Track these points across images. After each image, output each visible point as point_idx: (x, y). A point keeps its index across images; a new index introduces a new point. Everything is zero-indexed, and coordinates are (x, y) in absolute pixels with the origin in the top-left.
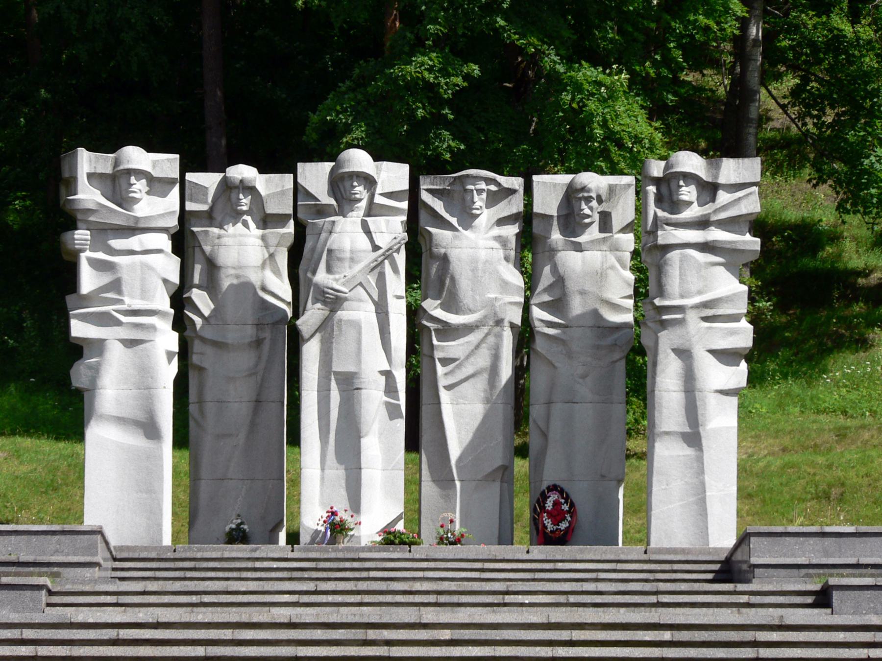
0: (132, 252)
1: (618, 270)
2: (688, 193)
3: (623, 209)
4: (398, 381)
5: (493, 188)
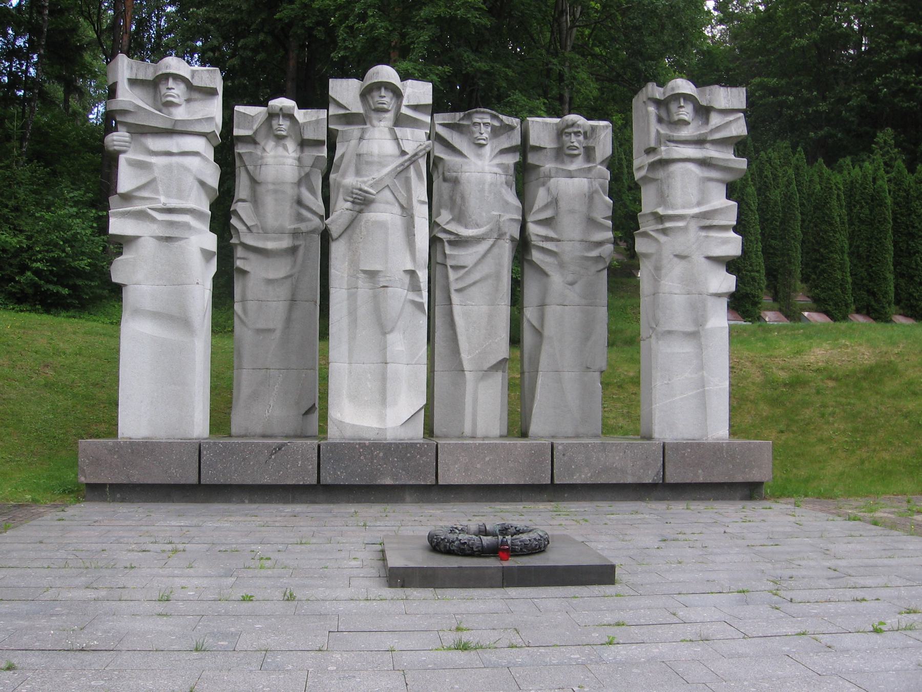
0: (169, 154)
1: (601, 194)
2: (686, 112)
3: (604, 145)
4: (421, 280)
5: (496, 124)
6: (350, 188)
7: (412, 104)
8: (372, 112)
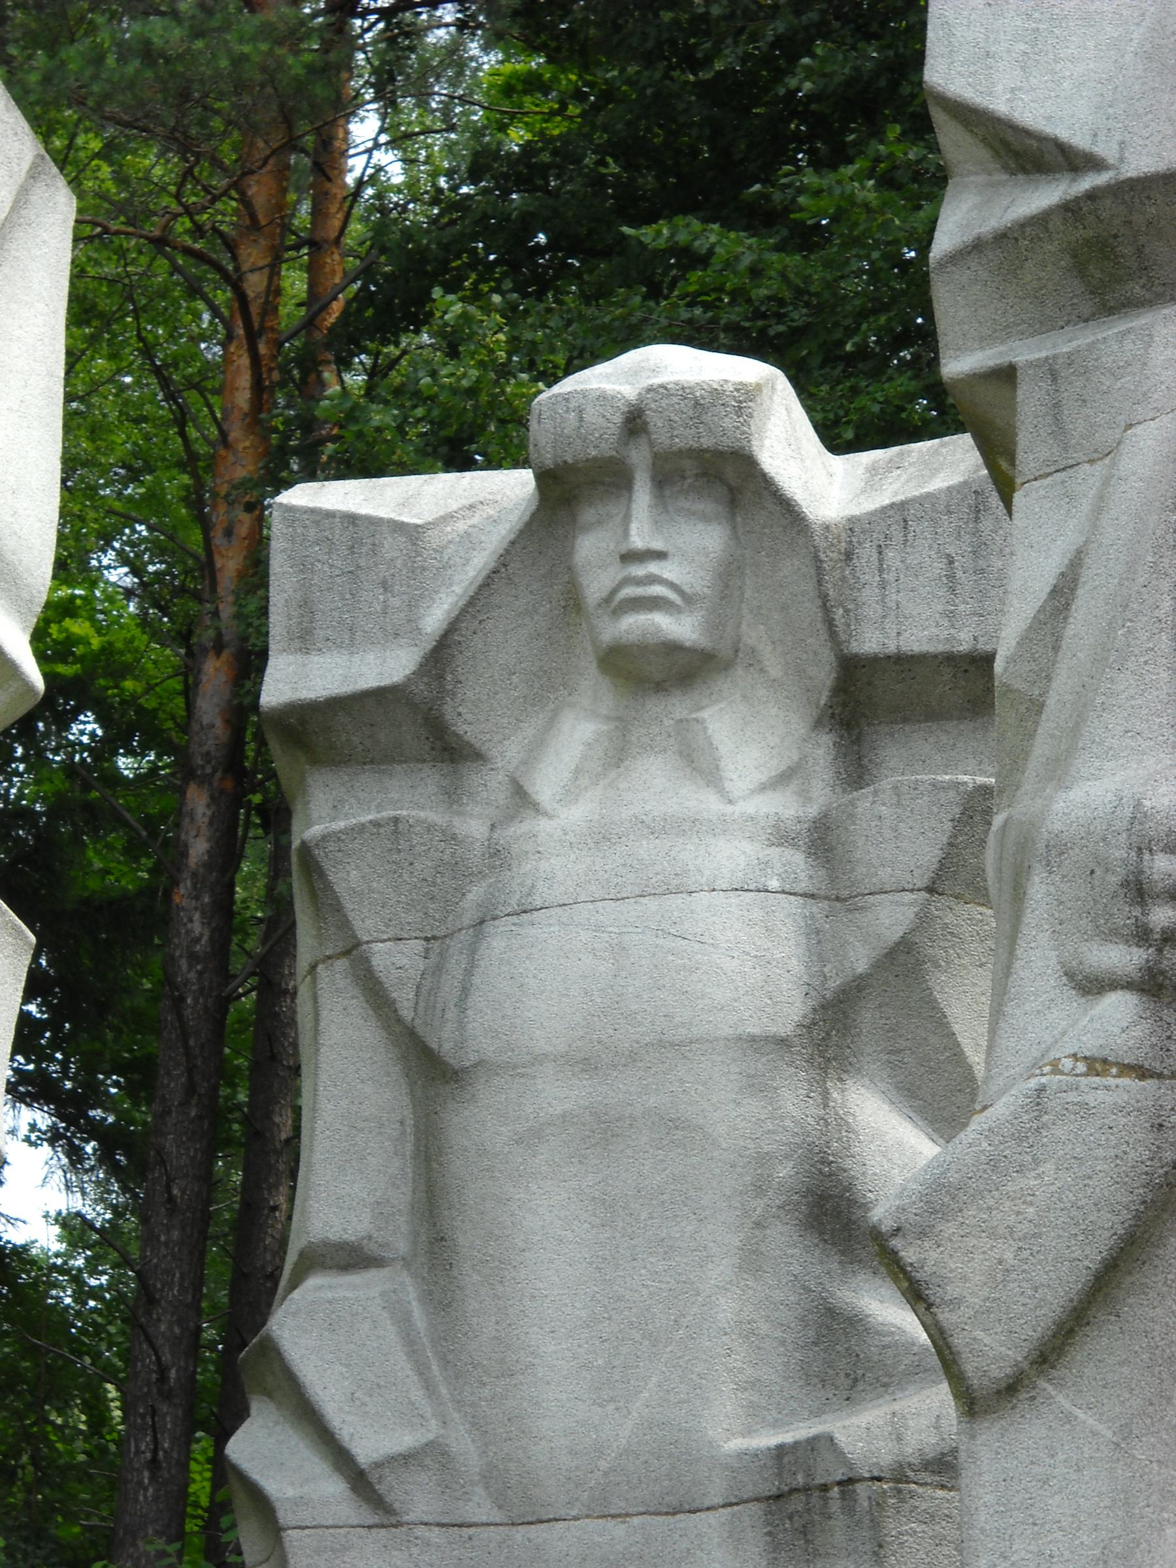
6: (1119, 853)
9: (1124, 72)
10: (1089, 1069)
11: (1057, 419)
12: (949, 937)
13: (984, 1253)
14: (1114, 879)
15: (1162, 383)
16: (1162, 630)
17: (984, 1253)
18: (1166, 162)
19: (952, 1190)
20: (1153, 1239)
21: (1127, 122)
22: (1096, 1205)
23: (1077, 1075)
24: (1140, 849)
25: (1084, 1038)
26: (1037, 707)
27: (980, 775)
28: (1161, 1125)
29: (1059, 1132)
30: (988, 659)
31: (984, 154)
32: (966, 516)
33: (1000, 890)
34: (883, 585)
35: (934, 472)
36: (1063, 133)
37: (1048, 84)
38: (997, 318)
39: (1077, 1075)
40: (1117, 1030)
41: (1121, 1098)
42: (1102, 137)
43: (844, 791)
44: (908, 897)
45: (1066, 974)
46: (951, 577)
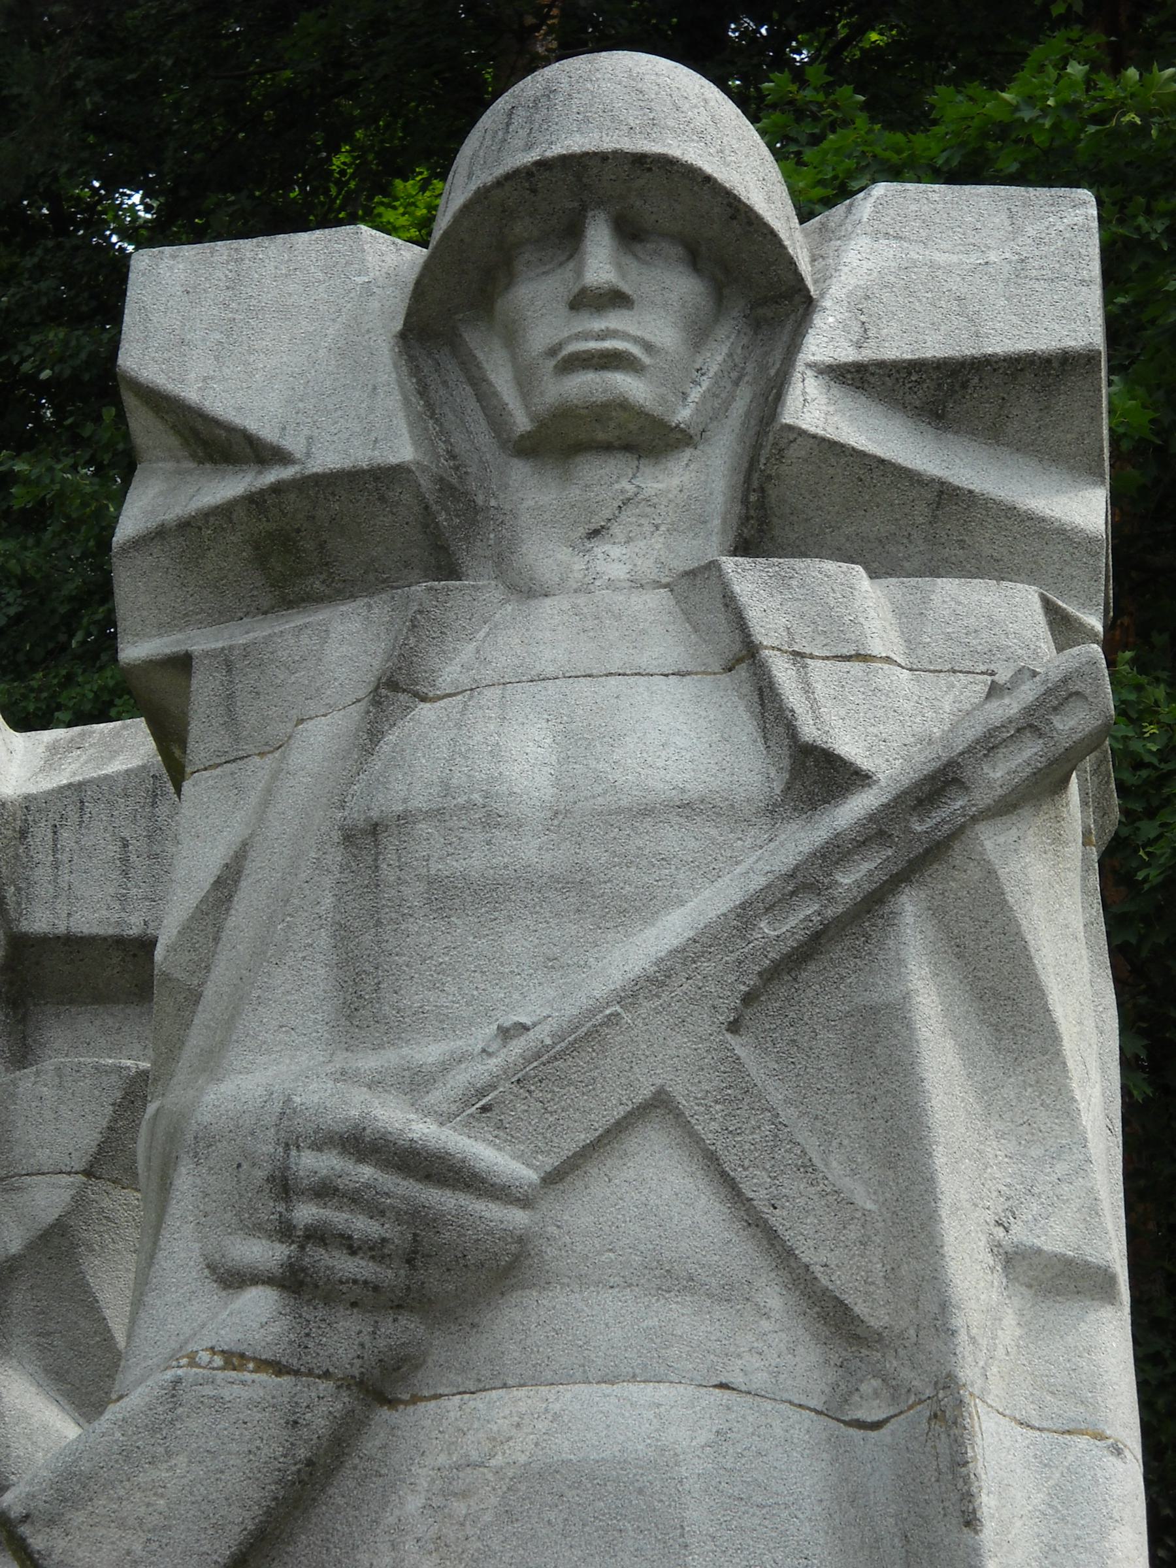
6: (266, 1148)
7: (891, 352)
8: (520, 471)
9: (317, 367)
10: (226, 1363)
11: (230, 712)
12: (104, 1222)
13: (113, 1543)
14: (260, 1174)
15: (335, 679)
16: (321, 926)
17: (113, 1543)
18: (352, 459)
19: (83, 1479)
20: (284, 1535)
21: (316, 417)
22: (227, 1499)
23: (214, 1369)
24: (287, 1145)
25: (223, 1332)
26: (195, 997)
27: (144, 1061)
28: (296, 1422)
29: (194, 1424)
30: (147, 945)
31: (173, 441)
32: (142, 801)
33: (148, 1178)
34: (56, 865)
35: (114, 755)
36: (252, 425)
37: (241, 375)
38: (177, 605)
39: (214, 1369)
40: (255, 1325)
41: (257, 1393)
42: (290, 431)
43: (7, 1069)
44: (65, 1179)
45: (208, 1266)
46: (125, 860)
